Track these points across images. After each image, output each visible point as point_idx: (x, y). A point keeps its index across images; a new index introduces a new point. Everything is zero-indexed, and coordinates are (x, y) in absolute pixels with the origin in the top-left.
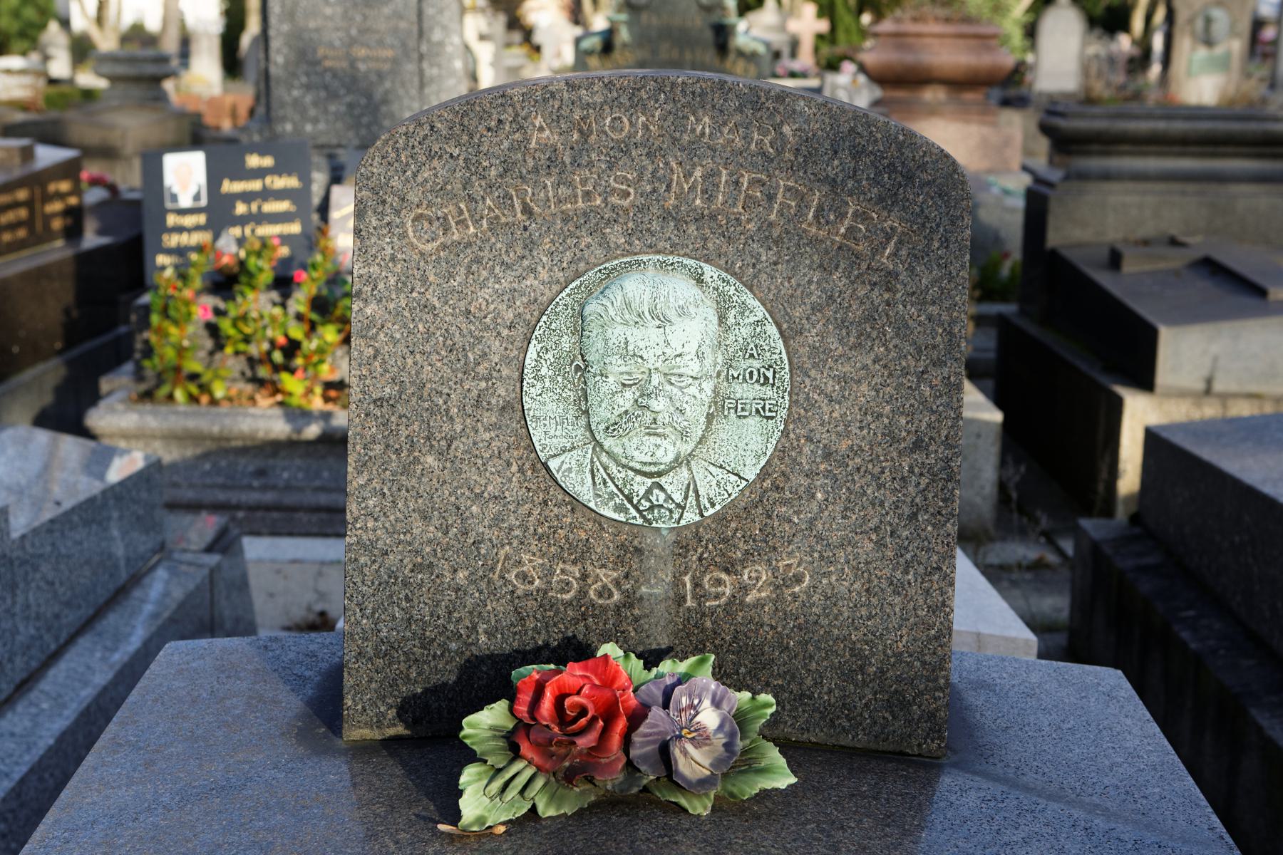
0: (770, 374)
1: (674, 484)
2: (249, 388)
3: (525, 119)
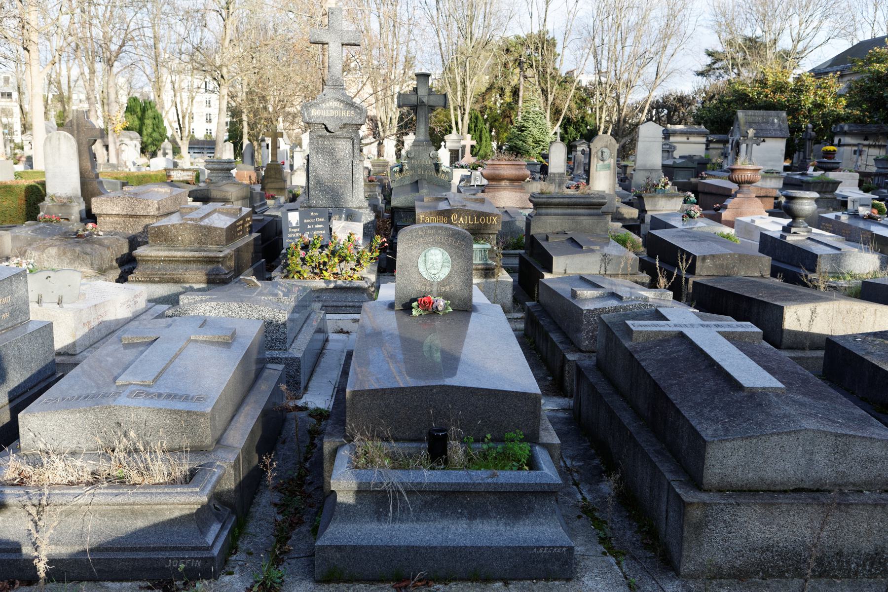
1: (437, 276)
2: (312, 275)
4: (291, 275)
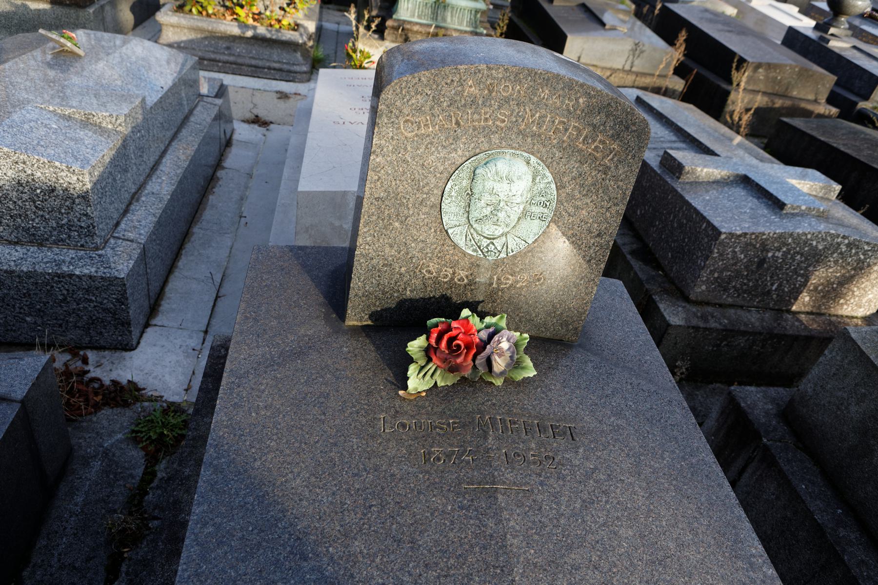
0: (548, 204)
1: (498, 244)
2: (222, 9)
3: (464, 81)
4: (187, 8)
